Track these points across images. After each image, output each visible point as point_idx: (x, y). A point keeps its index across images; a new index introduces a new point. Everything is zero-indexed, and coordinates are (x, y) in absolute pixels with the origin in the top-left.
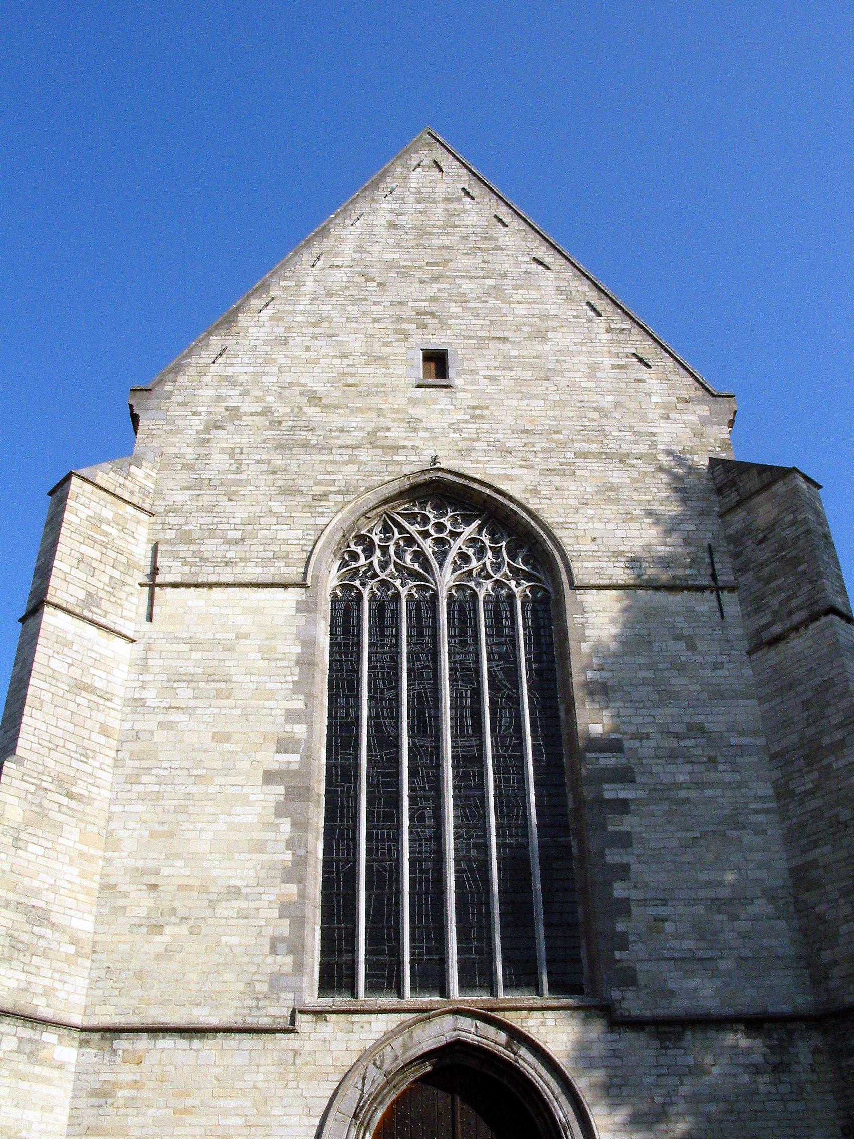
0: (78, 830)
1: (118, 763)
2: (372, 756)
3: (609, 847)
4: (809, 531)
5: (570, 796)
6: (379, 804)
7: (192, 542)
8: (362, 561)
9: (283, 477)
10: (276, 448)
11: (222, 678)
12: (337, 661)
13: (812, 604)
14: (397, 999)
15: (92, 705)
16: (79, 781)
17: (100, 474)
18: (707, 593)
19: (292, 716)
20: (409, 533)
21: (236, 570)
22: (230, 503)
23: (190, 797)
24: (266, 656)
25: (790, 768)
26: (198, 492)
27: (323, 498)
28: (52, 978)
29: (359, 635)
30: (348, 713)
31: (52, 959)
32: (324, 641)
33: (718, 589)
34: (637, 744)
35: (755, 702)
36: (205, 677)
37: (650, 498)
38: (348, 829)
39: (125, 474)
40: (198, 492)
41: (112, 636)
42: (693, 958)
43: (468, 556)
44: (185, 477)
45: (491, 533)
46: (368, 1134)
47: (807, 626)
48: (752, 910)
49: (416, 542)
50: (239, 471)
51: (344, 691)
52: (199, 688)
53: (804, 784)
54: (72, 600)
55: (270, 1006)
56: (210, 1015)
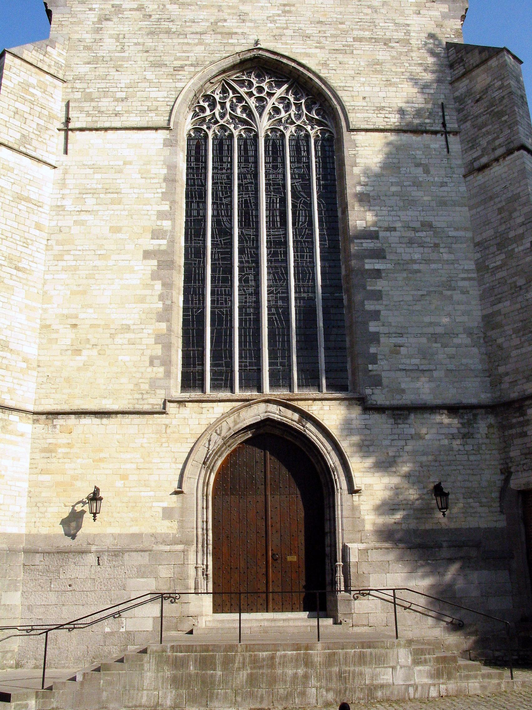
0: (24, 291)
1: (49, 248)
2: (215, 241)
3: (368, 299)
4: (511, 93)
5: (343, 267)
6: (219, 272)
7: (92, 100)
8: (208, 112)
9: (153, 55)
10: (148, 34)
11: (115, 191)
12: (191, 179)
13: (509, 143)
14: (231, 394)
15: (29, 210)
16: (23, 260)
17: (26, 52)
18: (439, 135)
19: (161, 215)
20: (239, 93)
21: (123, 118)
22: (117, 73)
23: (96, 268)
24: (144, 176)
25: (487, 252)
26: (95, 66)
27: (180, 69)
28: (12, 382)
29: (206, 162)
30: (198, 213)
31: (11, 371)
32: (183, 166)
33: (446, 133)
34: (388, 234)
35: (467, 208)
36: (104, 191)
37: (404, 70)
38: (199, 288)
39: (44, 53)
40: (95, 66)
41: (40, 164)
42: (418, 370)
43: (279, 109)
44: (86, 55)
45: (295, 94)
46: (212, 474)
47: (504, 158)
48: (456, 341)
49: (244, 99)
50: (123, 50)
51: (196, 199)
52: (100, 198)
53: (495, 262)
54: (11, 139)
55: (150, 398)
56: (113, 404)
